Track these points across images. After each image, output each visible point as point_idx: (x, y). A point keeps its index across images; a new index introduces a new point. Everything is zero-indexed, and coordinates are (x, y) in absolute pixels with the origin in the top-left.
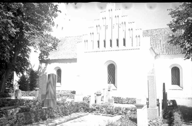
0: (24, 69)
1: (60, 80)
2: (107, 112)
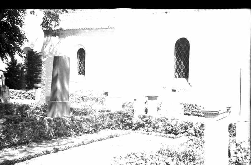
0: (13, 48)
1: (84, 71)
2: (166, 130)
